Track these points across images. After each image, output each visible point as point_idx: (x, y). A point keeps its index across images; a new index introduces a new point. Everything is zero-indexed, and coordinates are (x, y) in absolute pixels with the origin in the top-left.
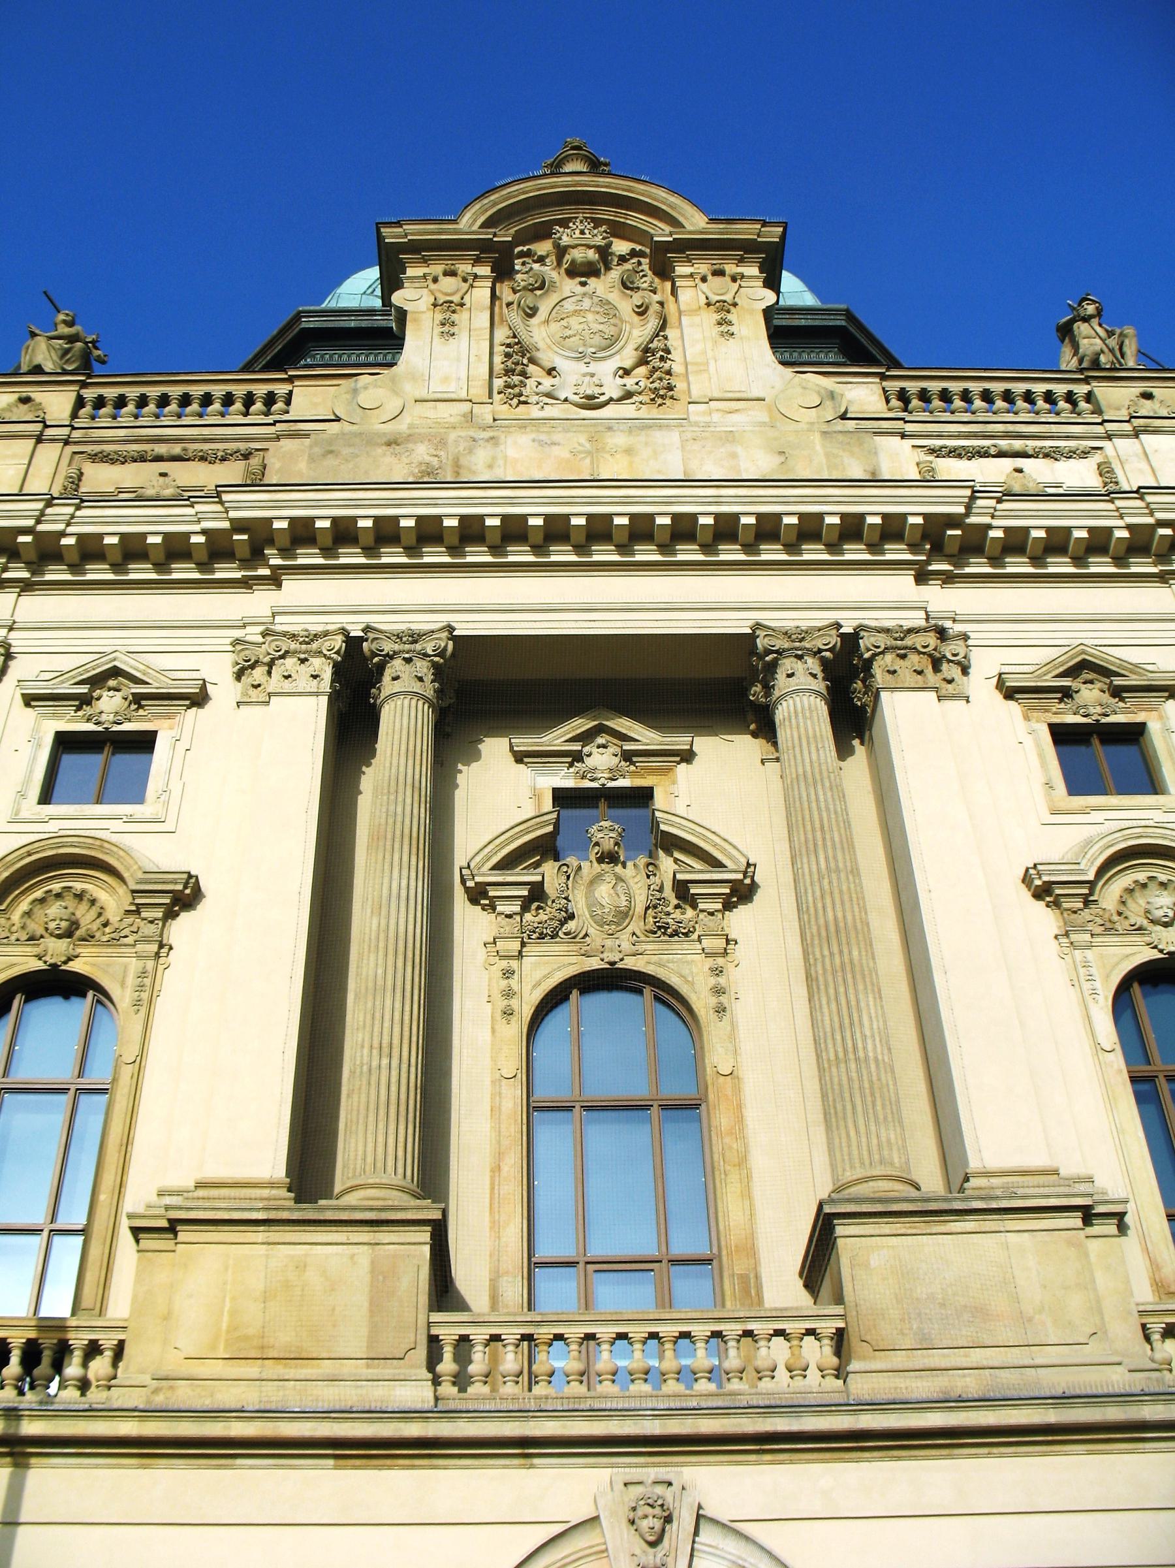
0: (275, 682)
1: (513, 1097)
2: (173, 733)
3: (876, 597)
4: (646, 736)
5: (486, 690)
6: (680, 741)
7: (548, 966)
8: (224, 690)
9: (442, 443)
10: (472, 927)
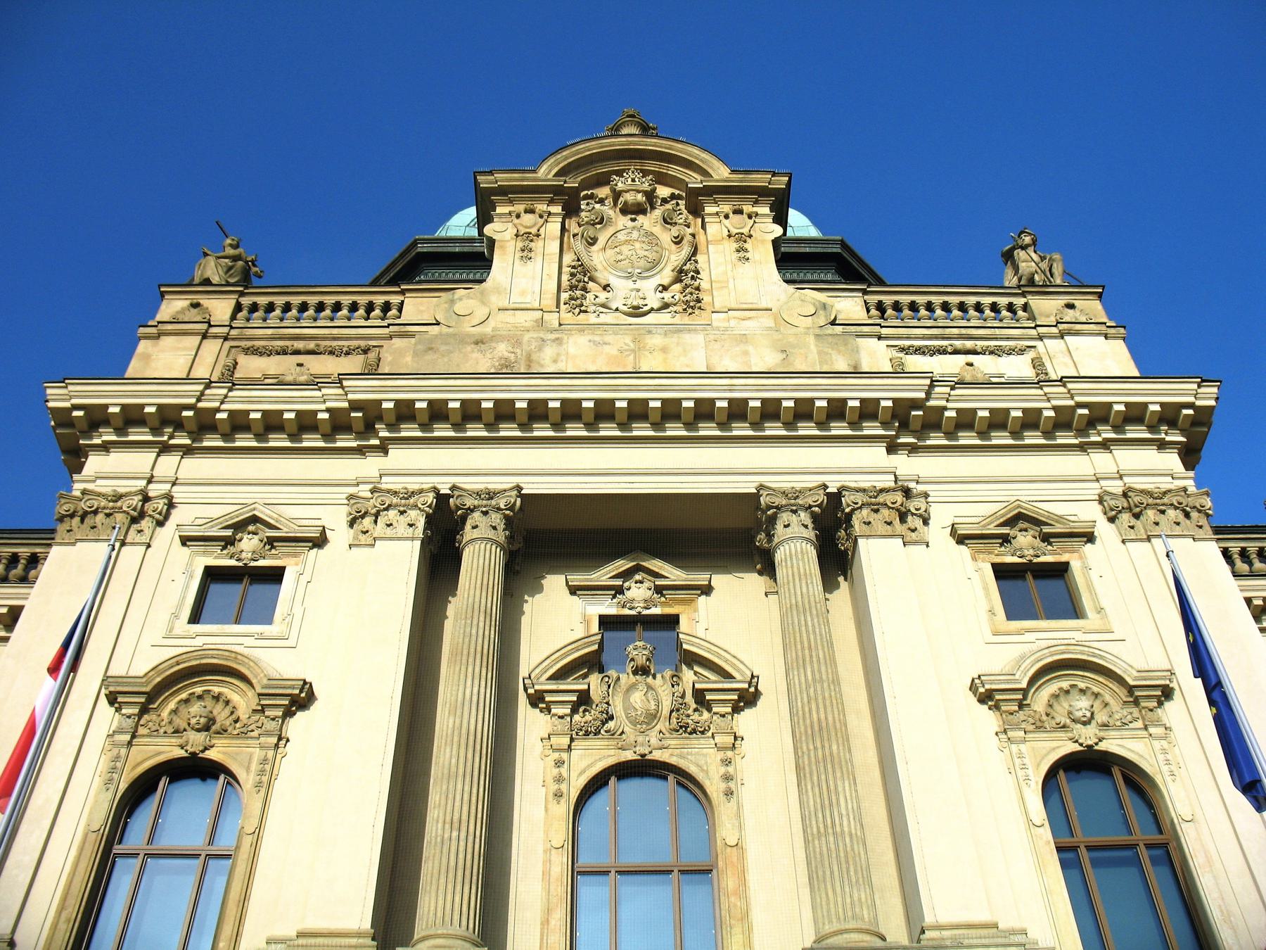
0: (380, 529)
1: (560, 863)
2: (299, 570)
3: (856, 464)
4: (673, 574)
5: (549, 537)
6: (700, 578)
7: (592, 757)
8: (340, 535)
9: (518, 343)
10: (532, 726)
